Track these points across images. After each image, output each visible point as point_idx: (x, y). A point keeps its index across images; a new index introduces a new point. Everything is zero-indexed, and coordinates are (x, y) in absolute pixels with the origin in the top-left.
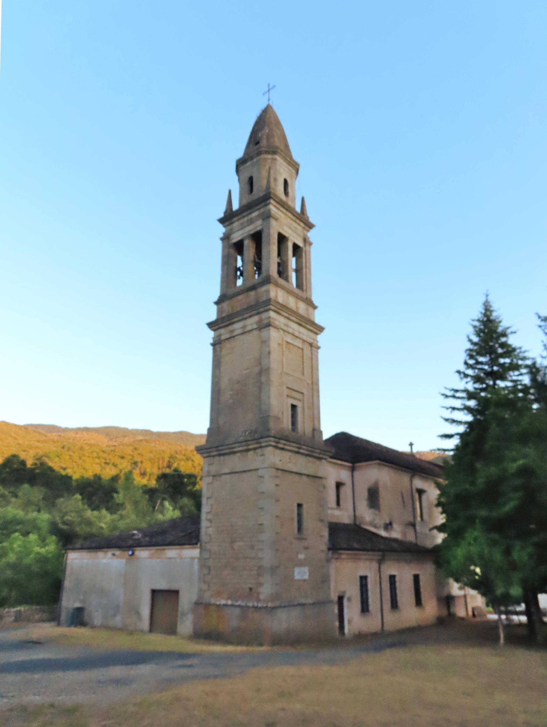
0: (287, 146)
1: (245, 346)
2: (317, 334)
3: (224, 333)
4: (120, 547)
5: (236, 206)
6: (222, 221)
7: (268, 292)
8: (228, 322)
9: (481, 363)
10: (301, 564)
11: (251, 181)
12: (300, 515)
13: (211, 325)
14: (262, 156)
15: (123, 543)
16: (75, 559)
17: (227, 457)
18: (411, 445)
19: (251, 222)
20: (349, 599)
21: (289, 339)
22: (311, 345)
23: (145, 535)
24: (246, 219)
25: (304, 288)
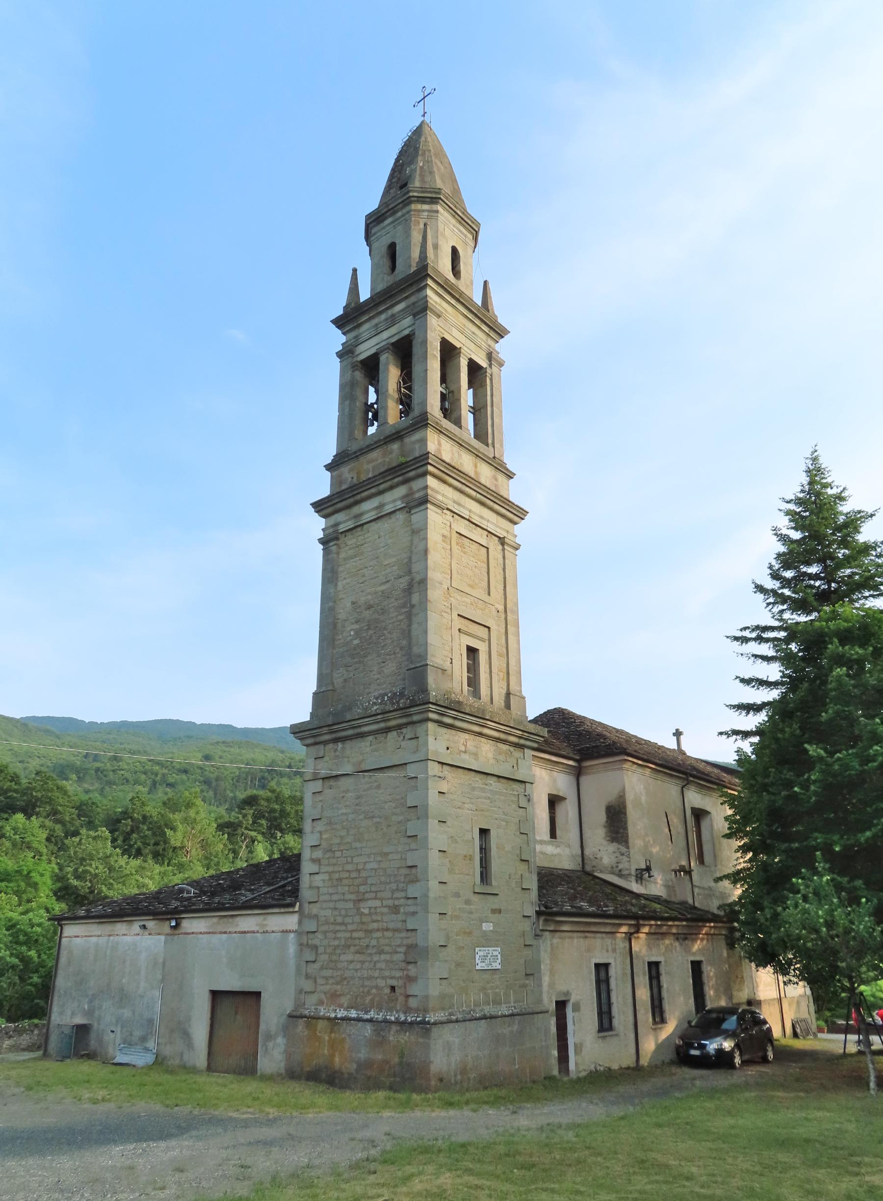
0: (457, 191)
1: (383, 540)
2: (515, 523)
3: (344, 520)
4: (156, 915)
5: (365, 294)
6: (340, 323)
7: (424, 441)
8: (351, 500)
9: (811, 577)
10: (487, 941)
11: (392, 250)
12: (484, 850)
13: (320, 506)
14: (413, 206)
15: (164, 908)
16: (79, 938)
17: (348, 744)
18: (678, 734)
19: (393, 321)
20: (577, 1008)
21: (462, 527)
22: (502, 541)
23: (203, 893)
24: (383, 317)
25: (490, 441)
